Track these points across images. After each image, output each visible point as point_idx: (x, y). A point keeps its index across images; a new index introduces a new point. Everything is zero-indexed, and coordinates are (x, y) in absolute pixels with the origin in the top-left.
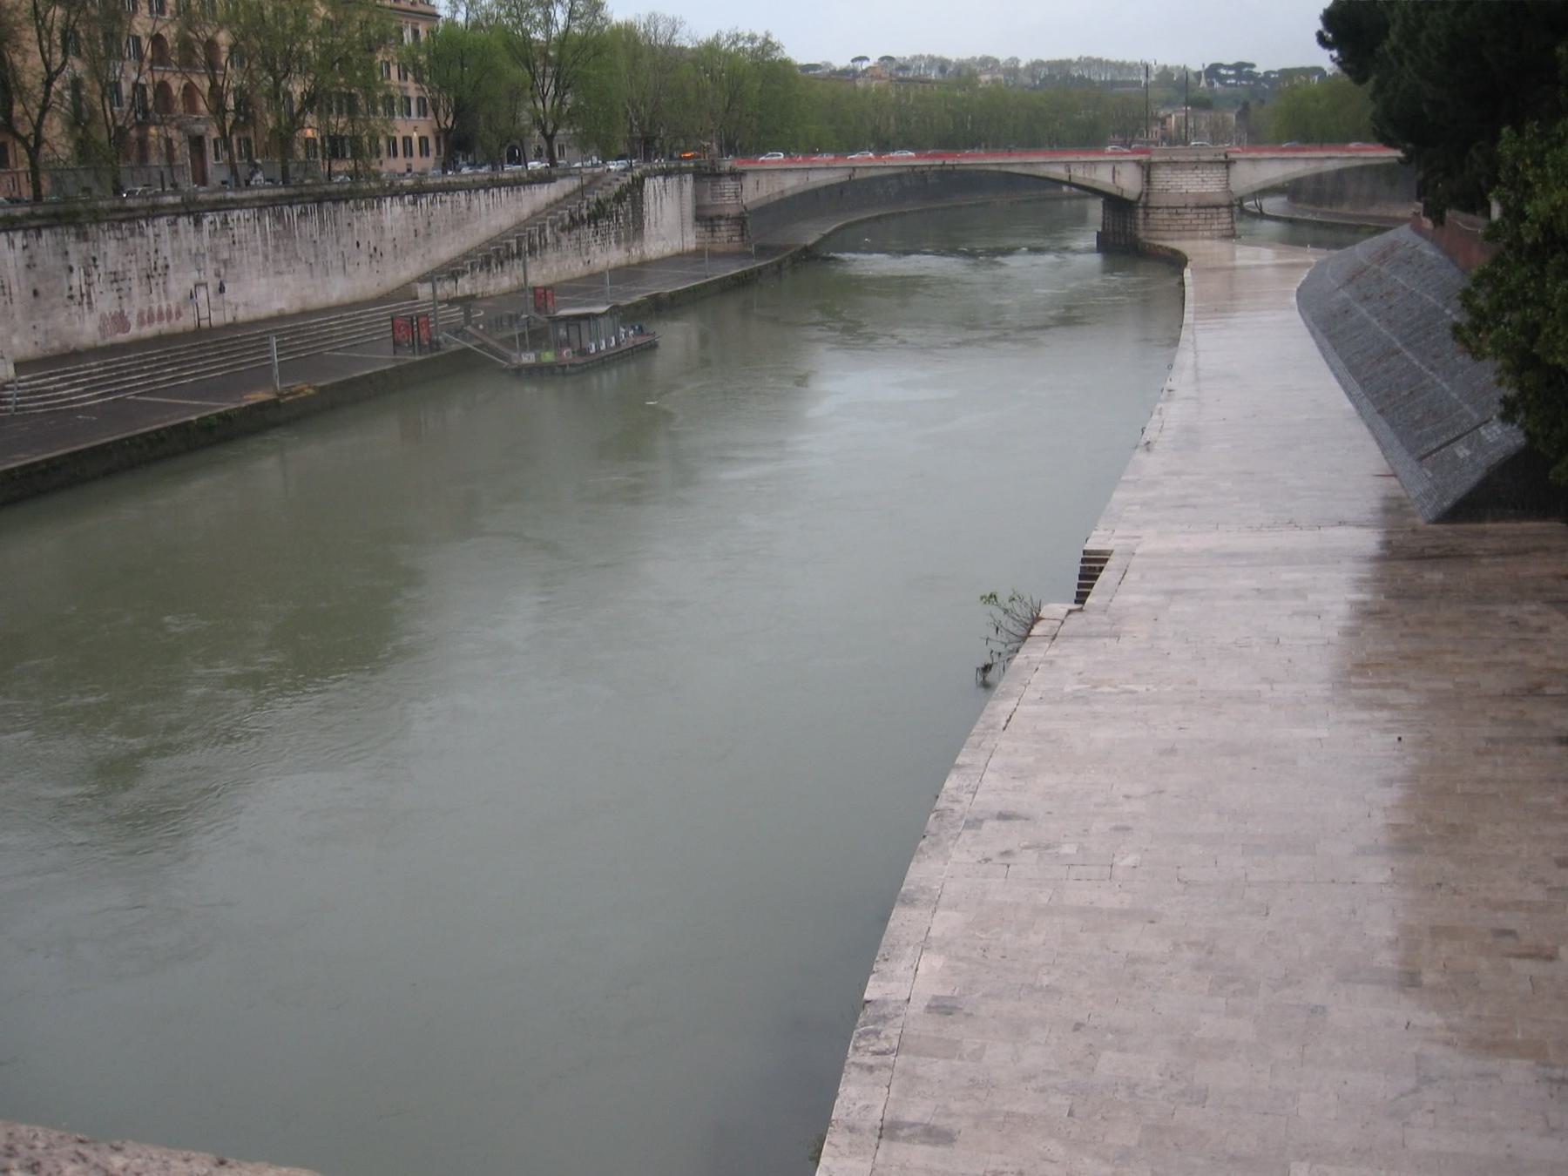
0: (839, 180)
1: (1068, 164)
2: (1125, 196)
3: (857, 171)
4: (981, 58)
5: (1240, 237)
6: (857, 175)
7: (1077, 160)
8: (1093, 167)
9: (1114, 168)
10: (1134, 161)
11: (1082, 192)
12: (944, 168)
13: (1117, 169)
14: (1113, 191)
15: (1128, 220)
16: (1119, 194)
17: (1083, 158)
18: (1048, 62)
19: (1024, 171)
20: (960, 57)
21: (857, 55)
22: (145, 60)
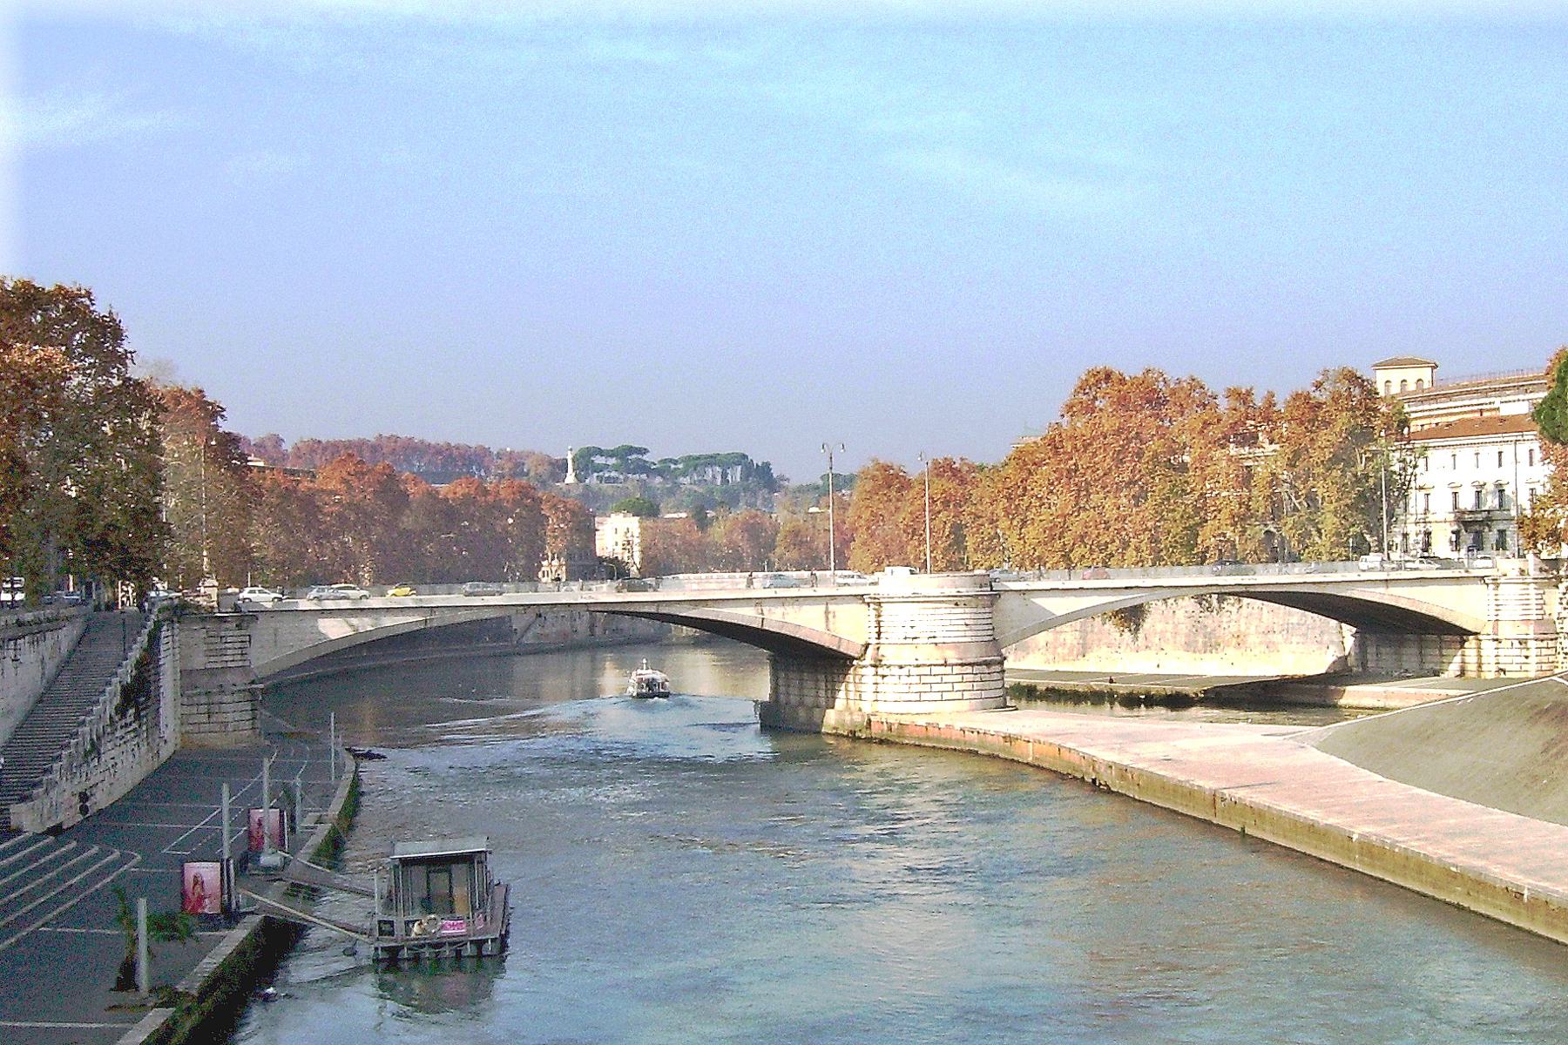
13: (830, 610)
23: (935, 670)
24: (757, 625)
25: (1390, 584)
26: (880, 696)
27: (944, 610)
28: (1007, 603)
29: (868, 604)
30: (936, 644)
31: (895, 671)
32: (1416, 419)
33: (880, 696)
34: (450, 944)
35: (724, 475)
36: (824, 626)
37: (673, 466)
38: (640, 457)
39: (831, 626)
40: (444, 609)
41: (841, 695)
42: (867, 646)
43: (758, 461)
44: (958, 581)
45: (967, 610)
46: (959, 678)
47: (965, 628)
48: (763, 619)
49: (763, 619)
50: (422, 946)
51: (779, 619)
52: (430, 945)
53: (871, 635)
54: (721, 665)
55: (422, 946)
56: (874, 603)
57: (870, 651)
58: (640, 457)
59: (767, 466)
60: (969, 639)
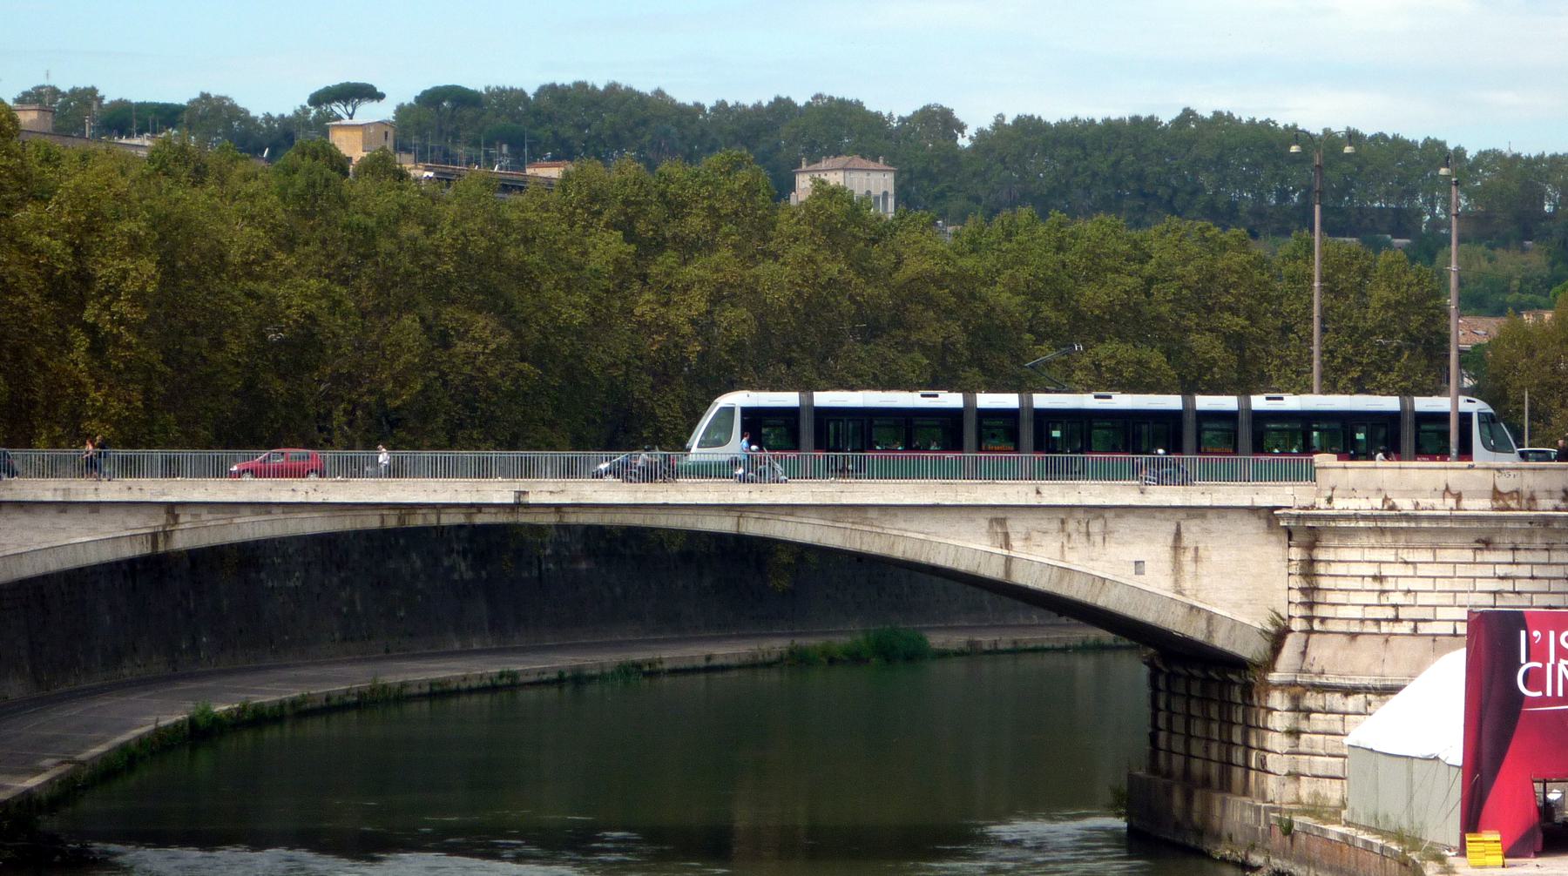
0: (107, 555)
1: (999, 516)
2: (1220, 641)
3: (185, 518)
4: (112, 103)
5: (868, 661)
6: (182, 540)
7: (1033, 500)
8: (1096, 527)
9: (1178, 535)
10: (1253, 510)
11: (1107, 637)
12: (525, 518)
13: (1188, 539)
14: (1175, 622)
15: (1237, 737)
16: (1200, 636)
17: (1057, 493)
18: (1491, 158)
19: (726, 525)
20: (77, 86)
21: (333, 80)
22: (521, 484)
39: (1187, 584)
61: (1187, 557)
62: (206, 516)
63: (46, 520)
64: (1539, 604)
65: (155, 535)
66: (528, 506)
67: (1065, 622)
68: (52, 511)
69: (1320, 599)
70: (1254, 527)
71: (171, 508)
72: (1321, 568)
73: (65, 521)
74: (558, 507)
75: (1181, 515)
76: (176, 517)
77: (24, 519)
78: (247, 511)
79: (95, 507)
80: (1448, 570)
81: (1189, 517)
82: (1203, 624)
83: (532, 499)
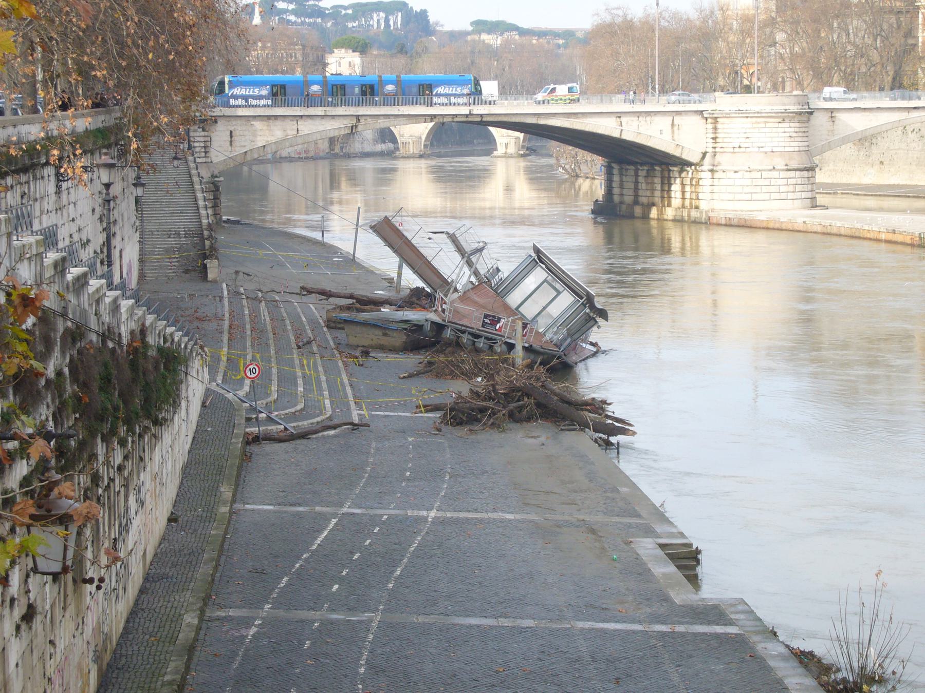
1: (619, 115)
3: (362, 120)
10: (696, 112)
13: (676, 122)
23: (765, 174)
24: (616, 134)
25: (304, 118)
26: (716, 196)
27: (773, 124)
28: (820, 120)
29: (706, 119)
30: (766, 153)
31: (732, 175)
32: (260, 97)
33: (716, 196)
34: (486, 338)
35: (387, 21)
36: (670, 137)
37: (344, 12)
38: (317, 3)
39: (676, 137)
40: (368, 118)
41: (676, 188)
42: (704, 154)
43: (417, 8)
44: (786, 100)
45: (792, 125)
46: (784, 181)
47: (789, 139)
48: (622, 130)
49: (622, 130)
50: (463, 332)
51: (606, 127)
52: (470, 333)
53: (708, 145)
54: (621, 175)
55: (463, 332)
56: (712, 118)
57: (708, 157)
58: (317, 3)
59: (424, 14)
60: (792, 149)
61: (676, 128)
62: (369, 120)
63: (318, 122)
64: (657, 119)
65: (352, 127)
66: (473, 114)
67: (842, 95)
68: (320, 118)
69: (856, 637)
70: (697, 119)
71: (358, 117)
72: (719, 131)
73: (324, 122)
74: (481, 115)
75: (674, 114)
76: (359, 120)
77: (310, 122)
78: (382, 117)
79: (333, 117)
80: (770, 130)
81: (676, 115)
82: (679, 150)
83: (475, 112)
